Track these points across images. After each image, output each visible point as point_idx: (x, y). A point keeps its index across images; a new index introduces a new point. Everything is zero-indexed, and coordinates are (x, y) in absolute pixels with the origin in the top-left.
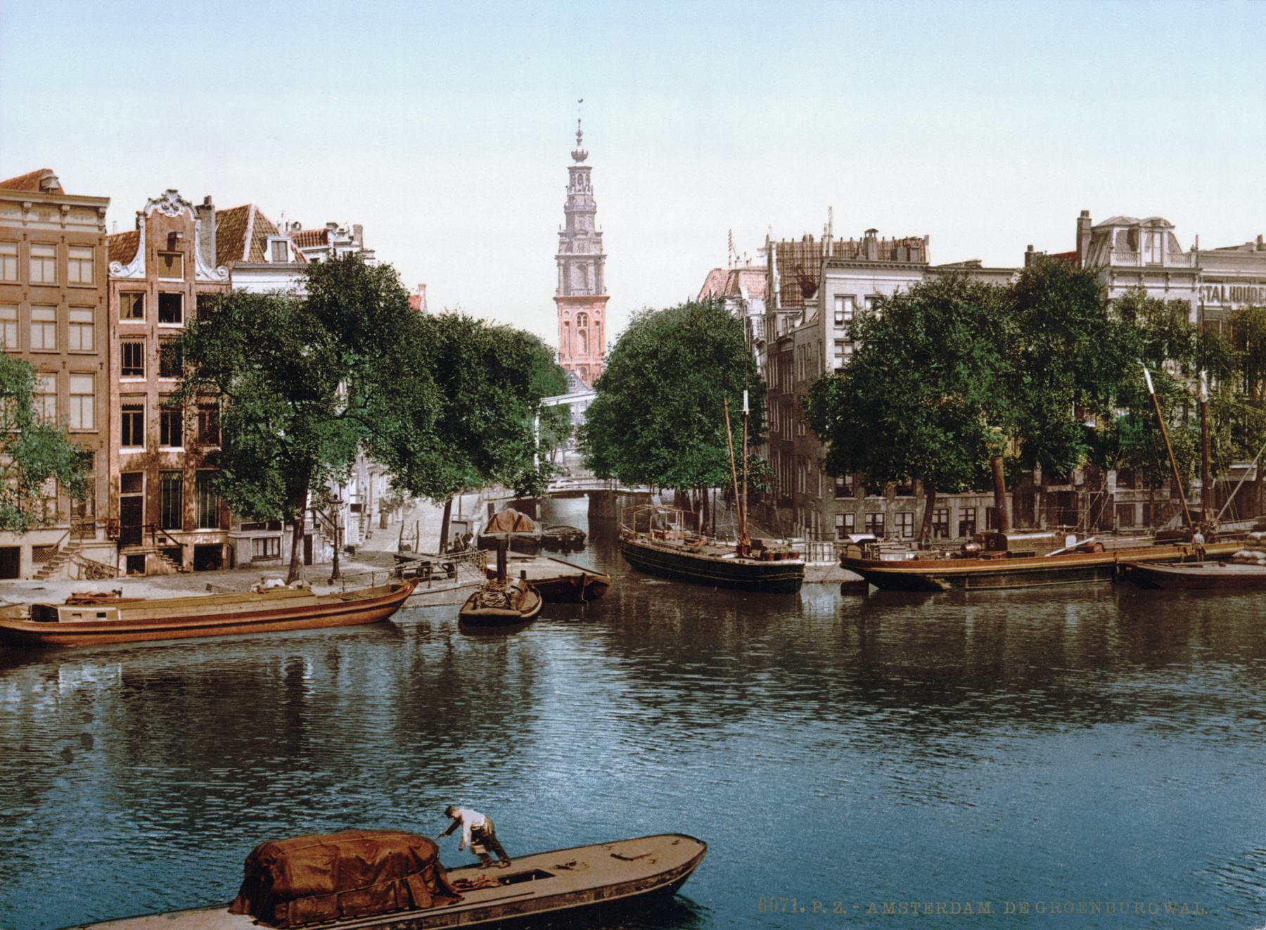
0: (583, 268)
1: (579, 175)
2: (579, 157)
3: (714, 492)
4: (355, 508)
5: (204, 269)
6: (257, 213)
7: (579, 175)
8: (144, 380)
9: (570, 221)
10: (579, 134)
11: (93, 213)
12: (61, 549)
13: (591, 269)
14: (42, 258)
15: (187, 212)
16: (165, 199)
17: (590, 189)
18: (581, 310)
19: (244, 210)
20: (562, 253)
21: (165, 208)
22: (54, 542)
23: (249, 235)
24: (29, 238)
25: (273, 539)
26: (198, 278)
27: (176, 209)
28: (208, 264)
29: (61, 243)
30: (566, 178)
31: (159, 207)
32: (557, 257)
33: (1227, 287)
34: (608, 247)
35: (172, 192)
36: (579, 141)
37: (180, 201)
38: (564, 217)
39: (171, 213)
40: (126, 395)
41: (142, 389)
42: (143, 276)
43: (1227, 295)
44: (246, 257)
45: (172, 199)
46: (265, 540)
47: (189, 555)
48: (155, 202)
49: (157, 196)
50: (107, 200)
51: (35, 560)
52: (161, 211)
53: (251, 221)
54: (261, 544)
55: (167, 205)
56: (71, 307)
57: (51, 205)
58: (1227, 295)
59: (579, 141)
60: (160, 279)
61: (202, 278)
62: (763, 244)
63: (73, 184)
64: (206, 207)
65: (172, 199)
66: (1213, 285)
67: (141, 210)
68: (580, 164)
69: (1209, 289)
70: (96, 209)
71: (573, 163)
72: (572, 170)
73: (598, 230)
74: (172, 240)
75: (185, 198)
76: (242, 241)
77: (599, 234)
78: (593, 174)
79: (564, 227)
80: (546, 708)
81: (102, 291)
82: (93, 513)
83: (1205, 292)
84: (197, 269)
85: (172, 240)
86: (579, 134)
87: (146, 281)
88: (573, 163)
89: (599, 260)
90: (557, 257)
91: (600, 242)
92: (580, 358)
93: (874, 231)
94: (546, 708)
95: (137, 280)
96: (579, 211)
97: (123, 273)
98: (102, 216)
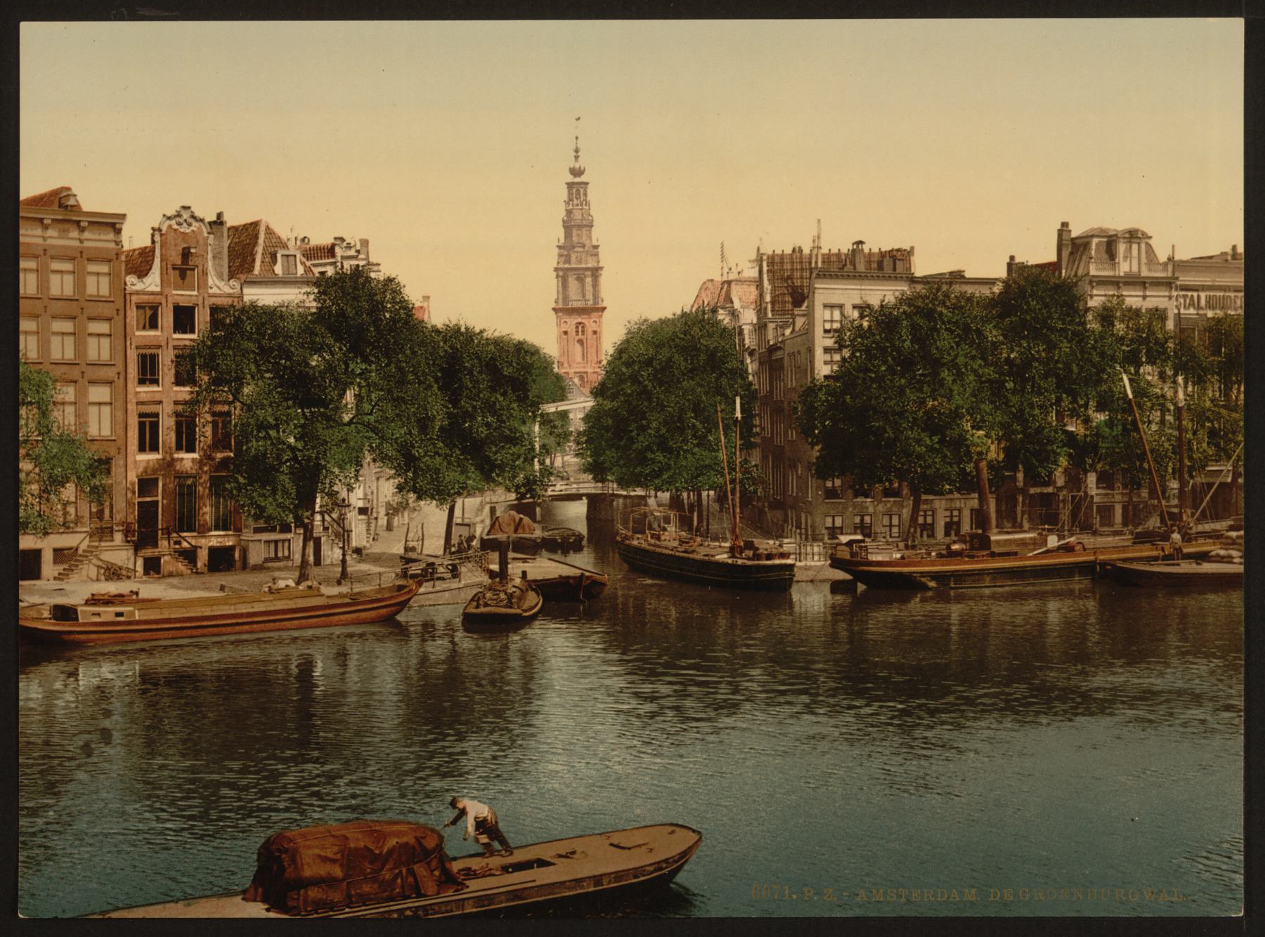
0: (581, 280)
1: (577, 190)
2: (577, 172)
5: (217, 282)
6: (268, 228)
7: (577, 190)
8: (160, 389)
9: (568, 235)
10: (577, 151)
11: (110, 229)
12: (80, 552)
13: (589, 280)
14: (61, 272)
15: (199, 228)
16: (179, 215)
17: (588, 204)
18: (579, 320)
19: (255, 225)
20: (561, 266)
21: (179, 224)
22: (75, 545)
23: (259, 249)
24: (49, 253)
25: (284, 541)
26: (211, 291)
27: (190, 225)
28: (220, 277)
29: (80, 257)
31: (173, 222)
32: (556, 269)
33: (1203, 295)
34: (605, 259)
35: (186, 208)
36: (577, 157)
37: (193, 217)
38: (562, 230)
39: (184, 229)
40: (143, 403)
41: (158, 398)
42: (158, 289)
43: (1203, 302)
45: (186, 215)
46: (276, 542)
47: (203, 556)
48: (169, 218)
50: (124, 216)
51: (56, 562)
52: (176, 227)
54: (272, 546)
56: (90, 319)
57: (69, 221)
58: (1203, 302)
59: (577, 157)
61: (215, 290)
62: (754, 256)
64: (218, 222)
65: (186, 215)
66: (1189, 294)
67: (156, 226)
68: (577, 180)
69: (1185, 297)
70: (113, 225)
71: (570, 178)
72: (570, 185)
73: (595, 243)
74: (186, 254)
75: (198, 214)
76: (253, 256)
77: (596, 247)
78: (590, 189)
79: (562, 240)
81: (120, 304)
82: (111, 517)
83: (1182, 300)
84: (210, 282)
85: (186, 254)
86: (577, 151)
87: (160, 293)
88: (570, 178)
89: (596, 272)
90: (556, 269)
91: (597, 255)
92: (578, 370)
96: (576, 225)
98: (118, 232)
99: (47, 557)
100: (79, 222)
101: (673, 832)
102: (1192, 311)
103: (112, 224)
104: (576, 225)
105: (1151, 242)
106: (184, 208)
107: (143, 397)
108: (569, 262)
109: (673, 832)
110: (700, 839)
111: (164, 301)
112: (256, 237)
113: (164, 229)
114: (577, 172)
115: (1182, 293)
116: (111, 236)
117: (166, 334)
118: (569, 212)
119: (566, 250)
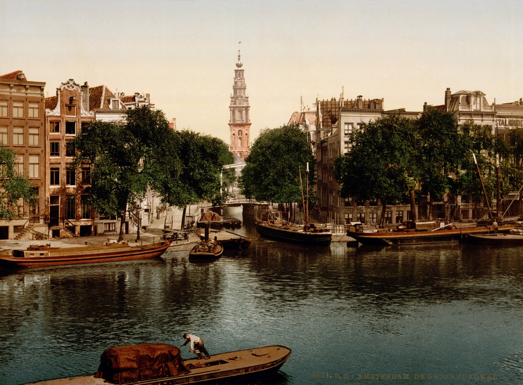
0: (240, 112)
1: (239, 73)
4: (146, 210)
5: (85, 112)
6: (106, 89)
7: (239, 73)
8: (60, 157)
9: (235, 92)
10: (239, 56)
11: (39, 89)
12: (25, 227)
13: (244, 112)
14: (18, 107)
15: (77, 88)
16: (68, 83)
18: (240, 129)
19: (101, 87)
21: (68, 87)
22: (23, 224)
23: (103, 98)
24: (12, 99)
25: (112, 223)
26: (82, 116)
27: (73, 87)
31: (66, 86)
32: (230, 107)
33: (507, 120)
36: (239, 59)
37: (74, 84)
38: (233, 90)
39: (71, 89)
40: (52, 164)
41: (59, 161)
42: (59, 115)
43: (507, 123)
45: (71, 83)
46: (109, 224)
48: (64, 84)
50: (45, 83)
51: (15, 232)
52: (67, 88)
54: (108, 225)
55: (69, 85)
58: (507, 123)
59: (239, 59)
62: (315, 102)
63: (30, 77)
64: (85, 86)
66: (502, 119)
67: (59, 88)
68: (239, 69)
69: (500, 120)
70: (40, 87)
71: (236, 68)
72: (236, 71)
73: (247, 96)
75: (77, 83)
78: (245, 73)
79: (233, 95)
84: (82, 112)
85: (71, 100)
86: (239, 56)
87: (60, 117)
88: (236, 68)
89: (247, 108)
90: (230, 107)
92: (240, 150)
93: (361, 96)
95: (57, 117)
96: (239, 88)
97: (51, 113)
98: (42, 90)
99: (11, 229)
101: (279, 349)
102: (503, 126)
103: (40, 87)
104: (239, 88)
105: (485, 97)
106: (71, 80)
107: (53, 161)
108: (235, 104)
109: (279, 349)
110: (290, 352)
112: (101, 93)
113: (62, 89)
115: (498, 119)
116: (39, 92)
117: (62, 134)
118: (236, 83)
119: (234, 99)
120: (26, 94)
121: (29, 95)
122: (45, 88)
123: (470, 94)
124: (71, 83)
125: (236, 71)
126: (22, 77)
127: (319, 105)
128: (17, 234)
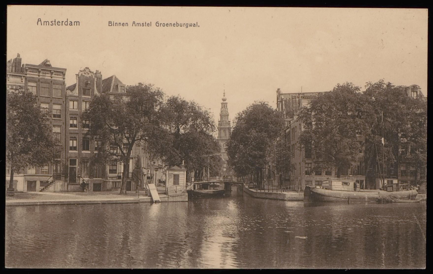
0: (225, 131)
2: (224, 100)
3: (390, 107)
4: (148, 178)
6: (115, 77)
8: (77, 129)
10: (224, 94)
13: (227, 131)
15: (92, 75)
17: (227, 109)
19: (112, 77)
21: (85, 73)
24: (40, 81)
25: (118, 182)
27: (88, 74)
30: (220, 106)
36: (224, 96)
37: (90, 72)
38: (220, 117)
39: (86, 75)
40: (71, 133)
41: (77, 132)
42: (77, 95)
44: (111, 91)
45: (87, 70)
46: (116, 182)
49: (82, 69)
50: (66, 70)
51: (41, 186)
52: (83, 74)
53: (113, 80)
54: (114, 183)
56: (54, 104)
57: (47, 70)
59: (224, 96)
60: (83, 96)
63: (55, 64)
67: (77, 74)
68: (224, 102)
71: (222, 102)
73: (229, 120)
75: (91, 70)
78: (228, 105)
79: (220, 120)
80: (203, 259)
81: (64, 99)
86: (224, 94)
87: (78, 97)
88: (222, 102)
94: (203, 259)
95: (74, 96)
98: (64, 75)
99: (38, 183)
100: (51, 71)
103: (62, 72)
105: (421, 90)
106: (86, 68)
111: (79, 99)
114: (224, 100)
118: (222, 112)
120: (52, 77)
121: (53, 78)
122: (66, 73)
123: (408, 87)
124: (87, 70)
125: (222, 103)
126: (48, 63)
127: (283, 102)
128: (42, 187)
